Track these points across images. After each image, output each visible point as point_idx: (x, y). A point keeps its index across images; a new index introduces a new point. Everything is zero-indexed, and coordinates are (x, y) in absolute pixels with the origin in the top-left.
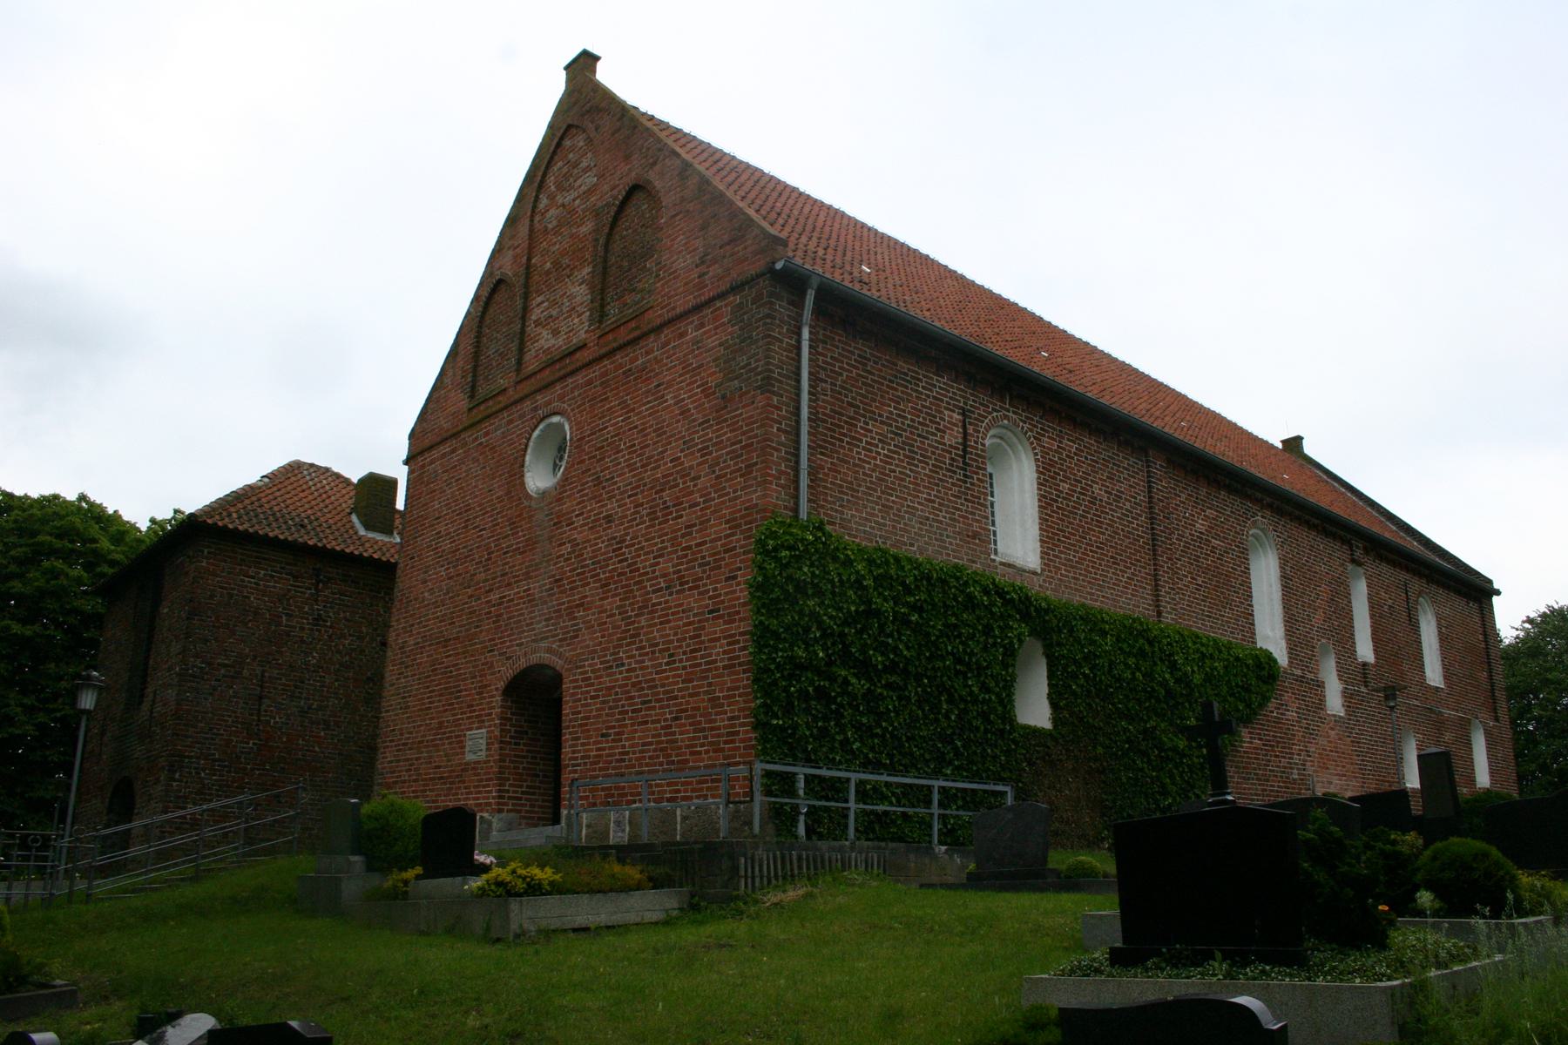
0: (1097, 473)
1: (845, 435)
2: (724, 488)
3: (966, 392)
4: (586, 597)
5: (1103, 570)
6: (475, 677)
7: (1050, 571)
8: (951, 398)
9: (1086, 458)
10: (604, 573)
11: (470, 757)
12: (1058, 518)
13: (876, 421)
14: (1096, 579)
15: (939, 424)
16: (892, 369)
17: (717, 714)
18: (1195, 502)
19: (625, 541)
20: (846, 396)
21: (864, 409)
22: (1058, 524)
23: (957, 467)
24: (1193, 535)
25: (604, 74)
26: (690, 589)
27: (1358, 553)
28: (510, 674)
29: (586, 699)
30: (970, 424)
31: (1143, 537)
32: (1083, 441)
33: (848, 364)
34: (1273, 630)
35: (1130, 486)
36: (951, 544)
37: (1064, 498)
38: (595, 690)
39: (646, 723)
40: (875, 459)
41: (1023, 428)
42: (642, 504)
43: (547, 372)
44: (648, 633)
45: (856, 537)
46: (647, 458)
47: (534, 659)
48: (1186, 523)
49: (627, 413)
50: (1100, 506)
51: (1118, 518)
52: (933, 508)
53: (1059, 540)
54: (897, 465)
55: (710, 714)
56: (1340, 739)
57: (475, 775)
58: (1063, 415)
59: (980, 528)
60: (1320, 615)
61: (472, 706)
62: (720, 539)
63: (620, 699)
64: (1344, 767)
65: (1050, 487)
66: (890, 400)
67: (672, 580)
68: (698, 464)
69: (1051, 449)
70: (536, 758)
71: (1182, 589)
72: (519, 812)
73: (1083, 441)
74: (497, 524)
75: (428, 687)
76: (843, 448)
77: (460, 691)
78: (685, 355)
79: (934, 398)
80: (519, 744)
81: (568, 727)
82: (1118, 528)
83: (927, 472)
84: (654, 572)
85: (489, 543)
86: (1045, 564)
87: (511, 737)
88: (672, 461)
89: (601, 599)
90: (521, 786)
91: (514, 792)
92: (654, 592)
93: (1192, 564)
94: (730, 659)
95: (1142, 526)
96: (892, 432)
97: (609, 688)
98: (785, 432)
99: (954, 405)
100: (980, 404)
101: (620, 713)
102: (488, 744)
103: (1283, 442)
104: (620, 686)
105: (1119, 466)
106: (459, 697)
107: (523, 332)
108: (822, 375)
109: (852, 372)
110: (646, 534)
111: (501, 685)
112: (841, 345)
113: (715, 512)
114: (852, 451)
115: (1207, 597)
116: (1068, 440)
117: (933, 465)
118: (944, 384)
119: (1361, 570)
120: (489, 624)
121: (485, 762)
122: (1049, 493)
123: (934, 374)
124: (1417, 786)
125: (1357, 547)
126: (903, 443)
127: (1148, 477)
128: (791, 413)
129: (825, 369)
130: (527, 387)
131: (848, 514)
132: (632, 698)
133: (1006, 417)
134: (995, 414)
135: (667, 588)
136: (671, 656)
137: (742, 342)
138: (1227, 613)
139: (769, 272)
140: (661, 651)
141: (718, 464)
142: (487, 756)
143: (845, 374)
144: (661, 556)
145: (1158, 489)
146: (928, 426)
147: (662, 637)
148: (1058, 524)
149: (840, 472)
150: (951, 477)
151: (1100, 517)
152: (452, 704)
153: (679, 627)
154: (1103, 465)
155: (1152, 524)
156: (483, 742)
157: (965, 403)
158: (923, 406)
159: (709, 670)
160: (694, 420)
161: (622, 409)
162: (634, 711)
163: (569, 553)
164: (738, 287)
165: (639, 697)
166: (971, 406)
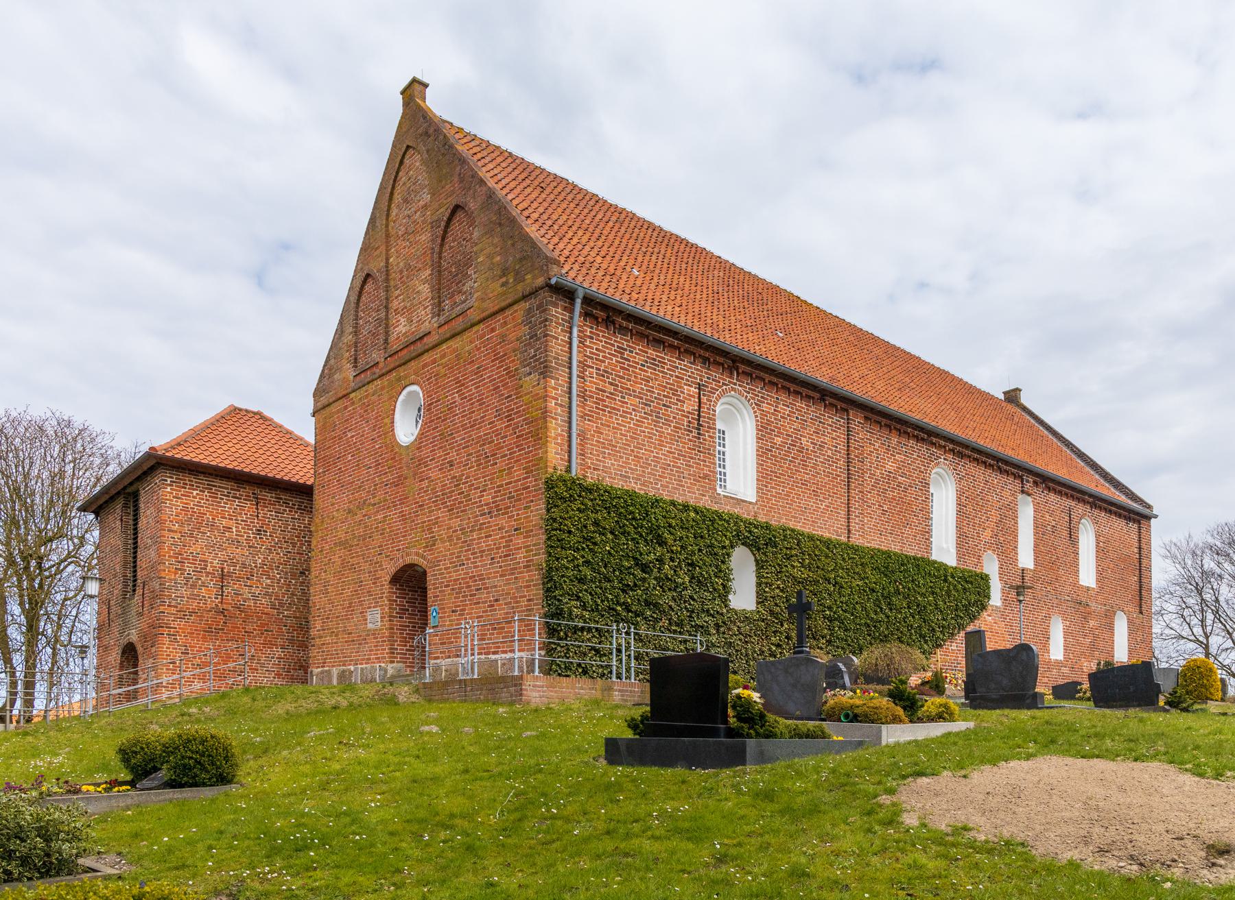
0: (806, 429)
1: (607, 406)
2: (522, 445)
3: (702, 372)
4: (439, 517)
5: (806, 500)
6: (371, 572)
7: (764, 502)
8: (689, 376)
9: (797, 418)
10: (450, 501)
11: (370, 626)
12: (771, 463)
13: (630, 395)
14: (799, 507)
15: (680, 396)
16: (644, 356)
17: (521, 597)
18: (886, 449)
19: (461, 480)
20: (608, 378)
21: (622, 387)
22: (771, 467)
23: (693, 427)
24: (883, 474)
25: (435, 103)
26: (503, 514)
27: (1028, 486)
28: (393, 570)
29: (441, 587)
30: (704, 395)
31: (840, 476)
32: (795, 405)
33: (609, 354)
34: (947, 542)
35: (833, 438)
36: (686, 483)
37: (777, 448)
38: (447, 581)
39: (479, 603)
40: (630, 423)
41: (746, 397)
42: (472, 454)
43: (405, 351)
44: (478, 543)
45: (614, 479)
46: (474, 421)
47: (408, 560)
48: (877, 465)
49: (459, 387)
50: (806, 453)
51: (821, 462)
52: (674, 457)
53: (771, 479)
54: (646, 428)
55: (516, 597)
56: (995, 623)
57: (374, 638)
58: (780, 386)
59: (710, 471)
60: (988, 533)
61: (370, 592)
62: (520, 480)
63: (463, 588)
64: (996, 642)
65: (767, 441)
66: (641, 379)
67: (492, 508)
68: (506, 427)
69: (769, 413)
70: (415, 627)
71: (870, 514)
72: (406, 662)
73: (795, 405)
74: (379, 464)
75: (340, 579)
76: (605, 416)
77: (362, 582)
78: (495, 346)
79: (677, 377)
80: (403, 618)
81: (431, 606)
82: (820, 470)
83: (669, 431)
84: (480, 501)
85: (374, 478)
86: (759, 496)
87: (397, 613)
88: (489, 424)
89: (450, 519)
90: (406, 646)
91: (400, 649)
92: (481, 515)
93: (880, 496)
94: (527, 561)
95: (841, 468)
96: (643, 403)
97: (455, 580)
98: (561, 406)
99: (692, 382)
100: (713, 380)
101: (463, 597)
102: (381, 617)
103: (1005, 393)
104: (462, 579)
105: (824, 424)
106: (361, 586)
107: (387, 318)
108: (589, 362)
109: (612, 360)
110: (475, 475)
111: (388, 578)
112: (604, 340)
113: (517, 461)
114: (611, 417)
115: (891, 520)
116: (783, 405)
117: (674, 427)
118: (685, 365)
119: (1030, 499)
120: (377, 535)
121: (380, 630)
122: (765, 445)
123: (676, 358)
124: (1060, 657)
125: (1028, 481)
126: (651, 411)
127: (848, 431)
128: (565, 392)
129: (592, 358)
130: (392, 362)
131: (608, 463)
132: (470, 586)
133: (733, 389)
134: (724, 387)
135: (489, 513)
136: (492, 559)
137: (531, 338)
138: (907, 531)
139: (547, 286)
140: (487, 555)
141: (518, 427)
142: (381, 626)
143: (607, 361)
144: (484, 491)
145: (855, 440)
146: (671, 398)
147: (487, 546)
148: (771, 467)
149: (602, 433)
150: (688, 435)
151: (806, 461)
152: (357, 590)
153: (496, 539)
154: (811, 423)
155: (848, 466)
156: (379, 616)
157: (701, 380)
158: (667, 383)
159: (516, 569)
160: (503, 395)
161: (456, 383)
162: (471, 595)
163: (427, 487)
164: (527, 296)
165: (474, 586)
166: (705, 382)
